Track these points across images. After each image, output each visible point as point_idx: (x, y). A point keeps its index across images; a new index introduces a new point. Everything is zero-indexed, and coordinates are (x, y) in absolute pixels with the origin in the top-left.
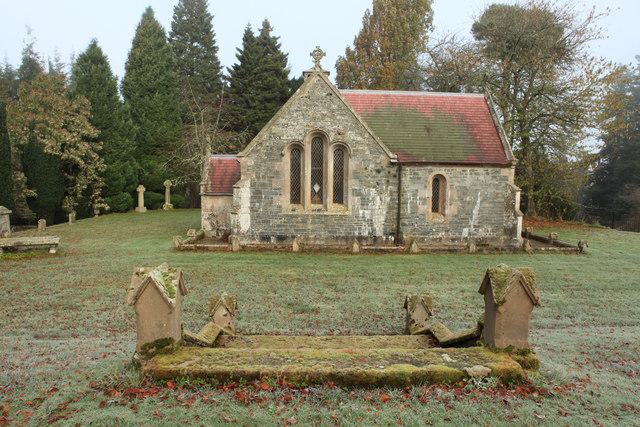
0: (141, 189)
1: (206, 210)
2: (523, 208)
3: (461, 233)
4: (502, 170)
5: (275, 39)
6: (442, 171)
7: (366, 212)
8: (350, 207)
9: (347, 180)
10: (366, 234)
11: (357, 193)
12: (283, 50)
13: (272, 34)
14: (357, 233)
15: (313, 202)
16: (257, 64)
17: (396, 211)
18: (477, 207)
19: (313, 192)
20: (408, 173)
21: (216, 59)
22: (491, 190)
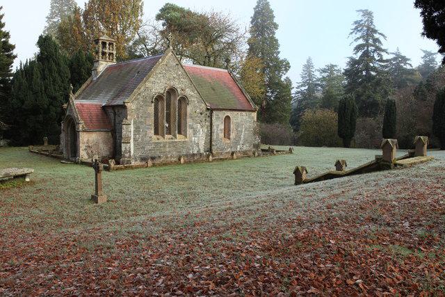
6: (228, 113)
10: (196, 152)
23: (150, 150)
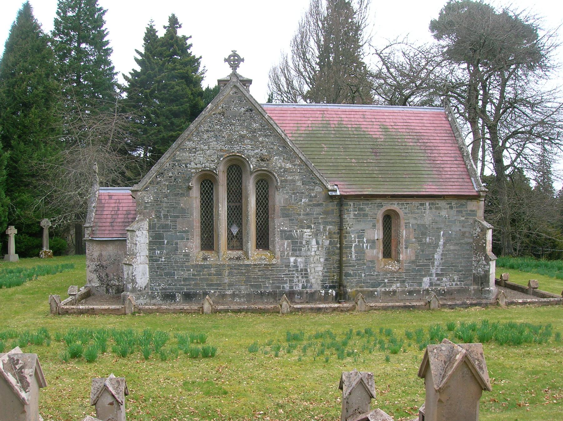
0: (12, 231)
1: (92, 260)
2: (497, 250)
3: (420, 284)
4: (469, 203)
5: (185, 38)
6: (395, 206)
7: (299, 260)
8: (278, 254)
9: (273, 219)
10: (299, 288)
11: (286, 235)
12: (194, 52)
13: (180, 33)
14: (287, 287)
15: (231, 247)
16: (161, 71)
17: (337, 258)
18: (440, 250)
19: (230, 237)
20: (351, 208)
21: (110, 63)
22: (457, 228)
23: (185, 280)
